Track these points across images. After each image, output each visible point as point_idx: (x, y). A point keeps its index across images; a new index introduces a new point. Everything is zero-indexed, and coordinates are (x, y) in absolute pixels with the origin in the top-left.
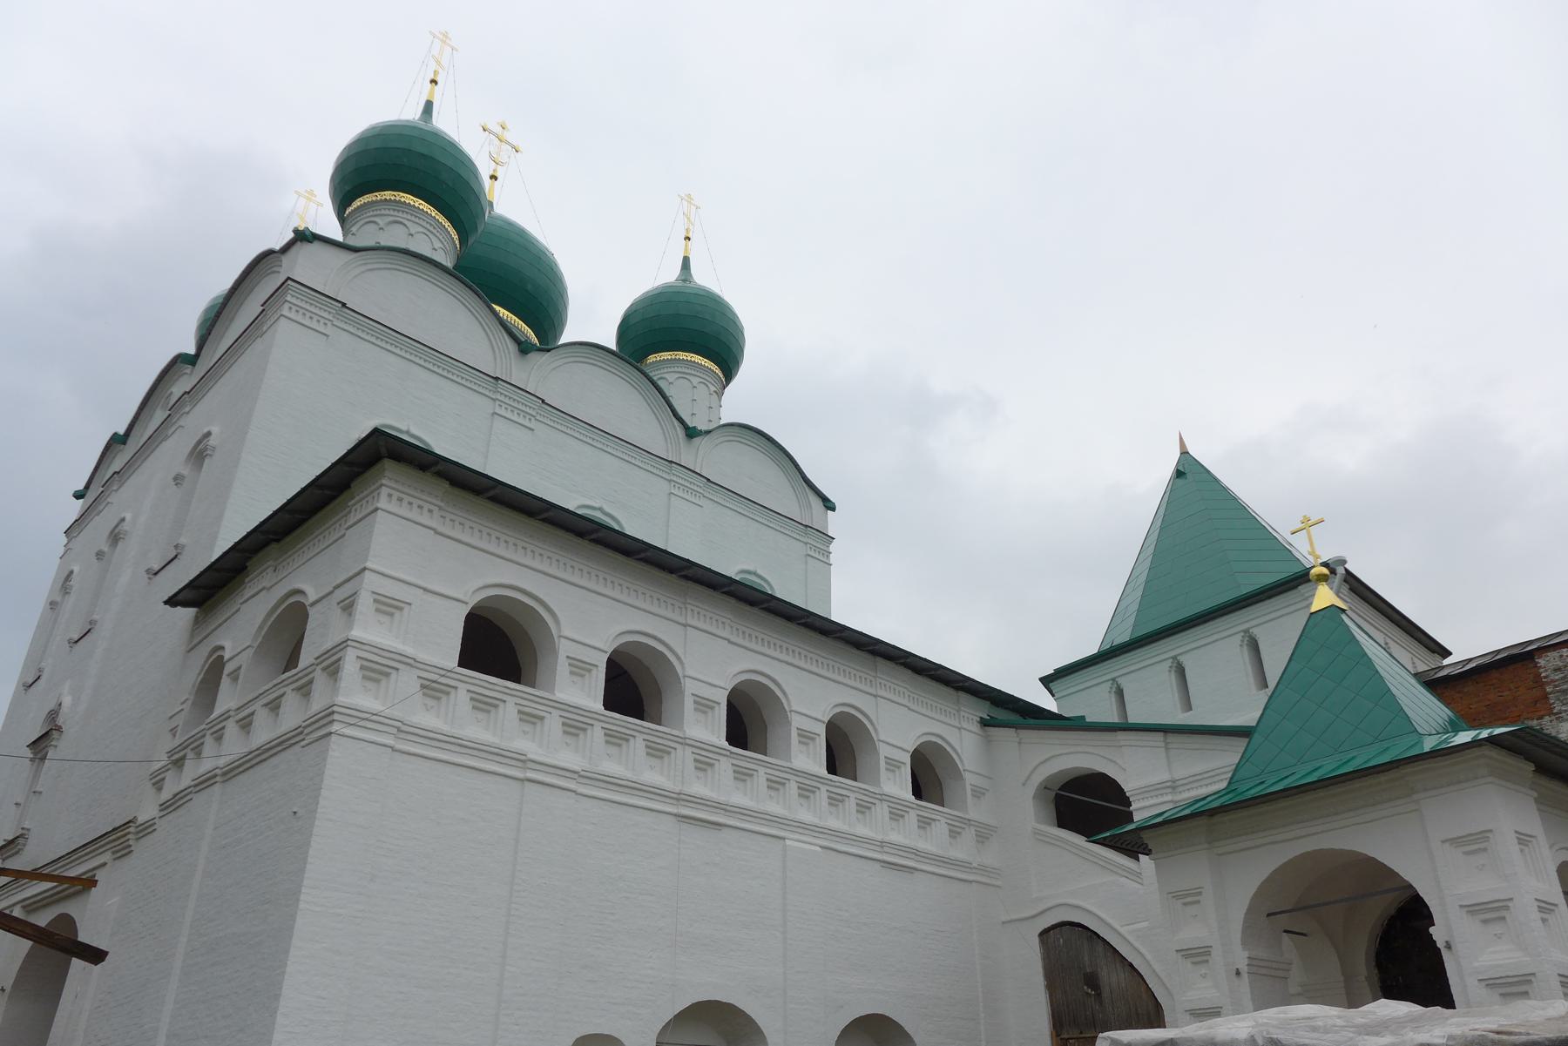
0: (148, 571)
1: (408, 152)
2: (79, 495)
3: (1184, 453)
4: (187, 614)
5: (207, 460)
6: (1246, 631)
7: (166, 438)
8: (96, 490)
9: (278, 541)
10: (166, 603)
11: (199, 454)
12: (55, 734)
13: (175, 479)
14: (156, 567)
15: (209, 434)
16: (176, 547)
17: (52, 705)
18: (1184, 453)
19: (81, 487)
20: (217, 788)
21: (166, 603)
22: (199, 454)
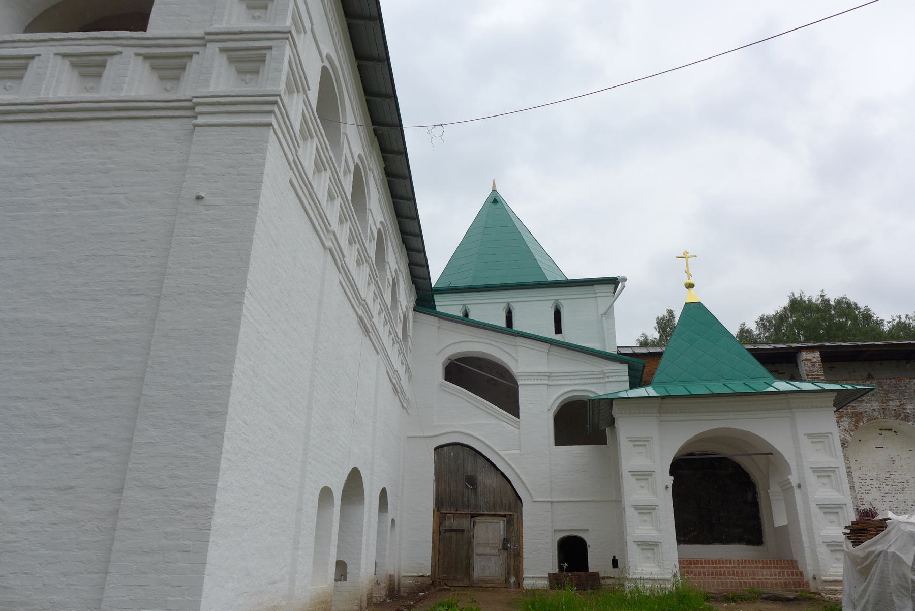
3: (494, 191)
6: (465, 305)
18: (494, 191)
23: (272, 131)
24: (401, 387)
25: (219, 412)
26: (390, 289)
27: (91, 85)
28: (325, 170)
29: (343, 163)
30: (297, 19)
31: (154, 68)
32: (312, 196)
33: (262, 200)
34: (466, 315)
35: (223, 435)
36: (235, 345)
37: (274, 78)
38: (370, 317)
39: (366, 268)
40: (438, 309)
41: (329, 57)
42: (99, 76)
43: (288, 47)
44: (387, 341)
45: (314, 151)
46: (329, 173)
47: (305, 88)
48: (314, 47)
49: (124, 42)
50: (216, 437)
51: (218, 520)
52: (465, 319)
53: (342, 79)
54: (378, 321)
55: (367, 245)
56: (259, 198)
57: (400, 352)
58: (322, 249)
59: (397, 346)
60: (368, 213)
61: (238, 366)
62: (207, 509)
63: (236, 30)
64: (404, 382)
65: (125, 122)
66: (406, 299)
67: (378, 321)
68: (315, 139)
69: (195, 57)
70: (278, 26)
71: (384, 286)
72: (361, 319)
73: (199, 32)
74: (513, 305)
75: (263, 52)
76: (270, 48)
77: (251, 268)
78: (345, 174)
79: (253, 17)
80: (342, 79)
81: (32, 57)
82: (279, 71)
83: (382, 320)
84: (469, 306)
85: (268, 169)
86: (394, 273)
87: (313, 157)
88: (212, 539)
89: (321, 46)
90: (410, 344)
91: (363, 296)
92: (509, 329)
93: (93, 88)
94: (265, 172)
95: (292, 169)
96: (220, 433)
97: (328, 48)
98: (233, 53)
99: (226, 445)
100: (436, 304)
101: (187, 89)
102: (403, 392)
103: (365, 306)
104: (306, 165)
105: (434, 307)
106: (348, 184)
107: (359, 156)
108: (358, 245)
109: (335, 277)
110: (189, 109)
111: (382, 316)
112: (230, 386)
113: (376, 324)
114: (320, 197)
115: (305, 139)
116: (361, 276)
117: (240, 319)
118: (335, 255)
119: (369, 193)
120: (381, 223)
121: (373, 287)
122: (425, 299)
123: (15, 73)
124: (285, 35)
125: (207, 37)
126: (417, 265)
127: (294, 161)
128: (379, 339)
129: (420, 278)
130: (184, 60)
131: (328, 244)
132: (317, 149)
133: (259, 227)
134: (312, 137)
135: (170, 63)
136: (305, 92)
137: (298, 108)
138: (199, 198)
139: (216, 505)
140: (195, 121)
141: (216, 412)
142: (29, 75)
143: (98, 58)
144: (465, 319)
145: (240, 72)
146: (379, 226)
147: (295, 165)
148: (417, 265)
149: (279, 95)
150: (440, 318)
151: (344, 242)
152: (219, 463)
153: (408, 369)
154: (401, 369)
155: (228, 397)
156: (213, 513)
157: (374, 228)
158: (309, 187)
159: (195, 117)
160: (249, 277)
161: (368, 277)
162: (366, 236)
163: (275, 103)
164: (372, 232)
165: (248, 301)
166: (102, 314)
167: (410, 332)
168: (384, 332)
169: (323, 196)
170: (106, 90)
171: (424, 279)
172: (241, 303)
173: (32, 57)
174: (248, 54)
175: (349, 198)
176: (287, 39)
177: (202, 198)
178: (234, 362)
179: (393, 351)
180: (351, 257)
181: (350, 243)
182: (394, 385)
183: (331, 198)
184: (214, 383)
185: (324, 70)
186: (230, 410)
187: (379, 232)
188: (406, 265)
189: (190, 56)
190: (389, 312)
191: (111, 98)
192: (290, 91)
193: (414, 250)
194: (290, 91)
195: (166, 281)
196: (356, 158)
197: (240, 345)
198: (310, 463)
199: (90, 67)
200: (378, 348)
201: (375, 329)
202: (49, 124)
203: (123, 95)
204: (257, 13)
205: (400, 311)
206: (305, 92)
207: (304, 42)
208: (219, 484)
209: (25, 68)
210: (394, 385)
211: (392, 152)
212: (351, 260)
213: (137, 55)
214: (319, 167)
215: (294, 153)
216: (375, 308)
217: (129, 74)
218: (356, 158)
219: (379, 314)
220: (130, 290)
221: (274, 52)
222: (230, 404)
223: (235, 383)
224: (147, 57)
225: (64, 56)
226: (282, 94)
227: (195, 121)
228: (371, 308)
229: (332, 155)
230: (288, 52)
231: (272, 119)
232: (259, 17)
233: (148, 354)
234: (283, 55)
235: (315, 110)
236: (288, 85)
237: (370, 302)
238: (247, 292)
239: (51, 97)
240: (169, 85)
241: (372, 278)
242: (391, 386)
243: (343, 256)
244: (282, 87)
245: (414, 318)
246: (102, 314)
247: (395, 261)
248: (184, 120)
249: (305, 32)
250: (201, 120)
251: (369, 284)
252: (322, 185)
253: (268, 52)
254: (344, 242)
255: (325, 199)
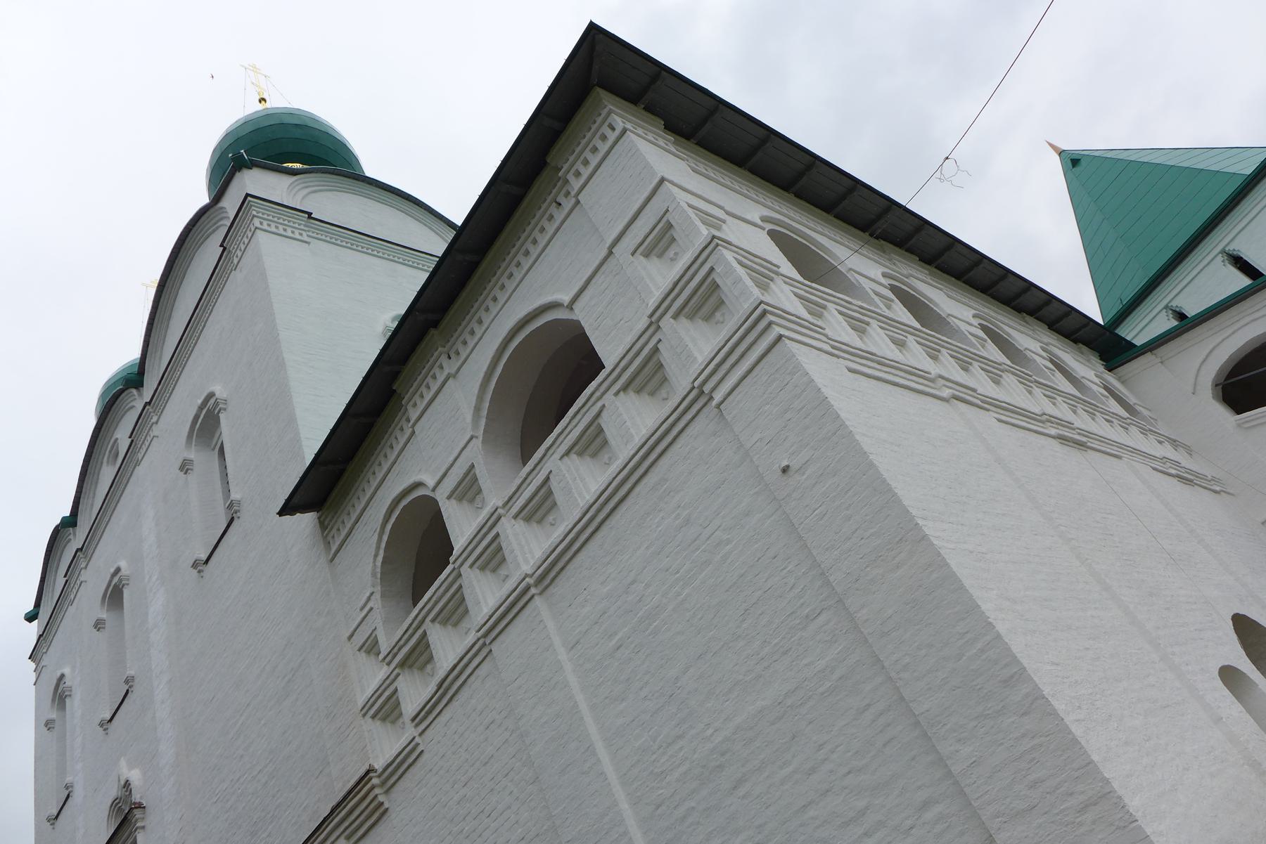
0: (101, 725)
1: (282, 125)
2: (31, 617)
3: (1061, 153)
4: (306, 521)
5: (67, 700)
6: (1166, 307)
7: (138, 463)
8: (47, 610)
9: (435, 324)
10: (281, 513)
11: (114, 596)
12: (138, 813)
13: (181, 468)
14: (204, 557)
15: (63, 676)
16: (67, 787)
17: (113, 792)
18: (1061, 153)
19: (30, 606)
20: (538, 601)
21: (281, 513)
22: (114, 596)
23: (787, 341)
24: (1189, 471)
25: (1016, 675)
26: (1058, 374)
27: (606, 456)
28: (868, 324)
29: (876, 299)
30: (708, 219)
31: (639, 391)
32: (882, 362)
33: (843, 415)
34: (1181, 316)
35: (1044, 697)
36: (961, 588)
37: (742, 292)
38: (1069, 425)
39: (1009, 379)
40: (1138, 342)
41: (764, 219)
42: (605, 442)
43: (725, 252)
44: (1114, 433)
45: (840, 317)
46: (874, 323)
47: (774, 269)
48: (744, 225)
49: (598, 394)
50: (1037, 702)
51: (1134, 803)
52: (1185, 323)
53: (794, 224)
54: (1082, 421)
55: (985, 354)
56: (838, 416)
57: (1144, 432)
58: (945, 404)
59: (1133, 429)
60: (950, 320)
61: (986, 607)
62: (1106, 797)
63: (671, 286)
64: (1185, 461)
65: (661, 462)
66: (1088, 369)
67: (1082, 421)
68: (830, 305)
69: (659, 346)
70: (699, 243)
71: (1048, 379)
72: (1060, 438)
73: (644, 322)
74: (1230, 248)
75: (709, 280)
76: (712, 269)
77: (899, 492)
78: (889, 307)
79: (672, 260)
80: (794, 224)
81: (547, 479)
82: (739, 280)
83: (1085, 415)
84: (1174, 304)
85: (819, 381)
86: (1044, 354)
87: (845, 324)
88: (1149, 831)
89: (749, 217)
90: (1145, 412)
91: (1037, 411)
92: (1260, 280)
93: (610, 459)
94: (820, 386)
95: (838, 357)
96: (1037, 697)
97: (755, 212)
98: (686, 310)
99: (1059, 706)
100: (1128, 338)
101: (681, 381)
102: (1197, 475)
103: (1059, 422)
104: (846, 339)
105: (1130, 345)
106: (901, 313)
107: (884, 275)
108: (976, 364)
109: (988, 420)
110: (699, 396)
111: (1080, 411)
112: (998, 636)
113: (1083, 427)
114: (890, 355)
115: (820, 316)
116: (1012, 391)
117: (939, 554)
118: (964, 397)
119: (930, 300)
120: (975, 316)
121: (1037, 391)
122: (1108, 345)
123: (548, 504)
124: (713, 243)
125: (654, 319)
126: (1060, 319)
127: (833, 347)
128: (1103, 440)
129: (1080, 329)
130: (655, 359)
131: (946, 393)
132: (841, 313)
133: (866, 444)
134: (824, 307)
135: (647, 373)
136: (777, 274)
137: (786, 295)
138: (785, 470)
139: (1115, 785)
140: (714, 403)
141: (1012, 677)
142: (558, 496)
143: (592, 428)
144: (1185, 323)
145: (708, 318)
146: (976, 322)
147: (838, 350)
148: (1060, 319)
149: (762, 302)
150: (1151, 350)
151: (957, 374)
152: (1070, 732)
153: (1174, 443)
154: (1167, 451)
155: (1009, 649)
156: (1120, 798)
157: (973, 330)
158: (870, 356)
159: (711, 398)
160: (906, 503)
161: (1021, 386)
162: (973, 345)
163: (764, 313)
164: (877, 294)
165: (929, 528)
166: (805, 662)
167: (1132, 400)
168: (1099, 427)
169: (891, 352)
170: (623, 449)
171: (1085, 326)
172: (925, 537)
173: (547, 479)
174: (699, 296)
175: (918, 325)
176: (717, 245)
177: (788, 466)
178: (978, 606)
179: (1134, 438)
180: (979, 381)
181: (966, 370)
182: (1178, 476)
183: (901, 344)
184: (979, 645)
185: (772, 234)
186: (1025, 662)
187: (983, 328)
188: (1048, 332)
189: (656, 350)
190: (1083, 399)
191: (632, 452)
192: (764, 288)
193: (1040, 308)
194: (764, 288)
195: (832, 579)
196: (883, 280)
197: (967, 583)
198: (1173, 654)
199: (593, 443)
200: (1115, 451)
201: (1087, 434)
202: (607, 523)
203: (637, 441)
204: (671, 253)
205: (1095, 388)
206: (777, 274)
207: (733, 232)
208: (1095, 757)
209: (550, 493)
210: (1178, 476)
211: (941, 253)
212: (986, 387)
213: (616, 394)
214: (860, 327)
215: (825, 339)
216: (1062, 411)
217: (629, 418)
218: (883, 280)
219: (1075, 412)
220: (807, 616)
221: (718, 270)
222: (1018, 655)
223: (1001, 628)
224: (625, 388)
225: (567, 453)
226: (763, 298)
227: (714, 403)
228: (1059, 415)
229: (860, 303)
230: (729, 255)
231: (777, 330)
232: (676, 254)
233: (883, 667)
234: (728, 264)
235: (801, 279)
236: (759, 285)
237: (1050, 409)
238: (920, 522)
239: (589, 498)
240: (663, 393)
241: (1027, 381)
242: (1175, 481)
243: (974, 390)
244: (756, 292)
245: (1119, 379)
246: (805, 662)
247: (1032, 340)
248: (705, 410)
249: (724, 222)
250: (718, 396)
251: (1030, 393)
252: (879, 341)
253: (713, 275)
254: (957, 374)
255: (897, 351)
